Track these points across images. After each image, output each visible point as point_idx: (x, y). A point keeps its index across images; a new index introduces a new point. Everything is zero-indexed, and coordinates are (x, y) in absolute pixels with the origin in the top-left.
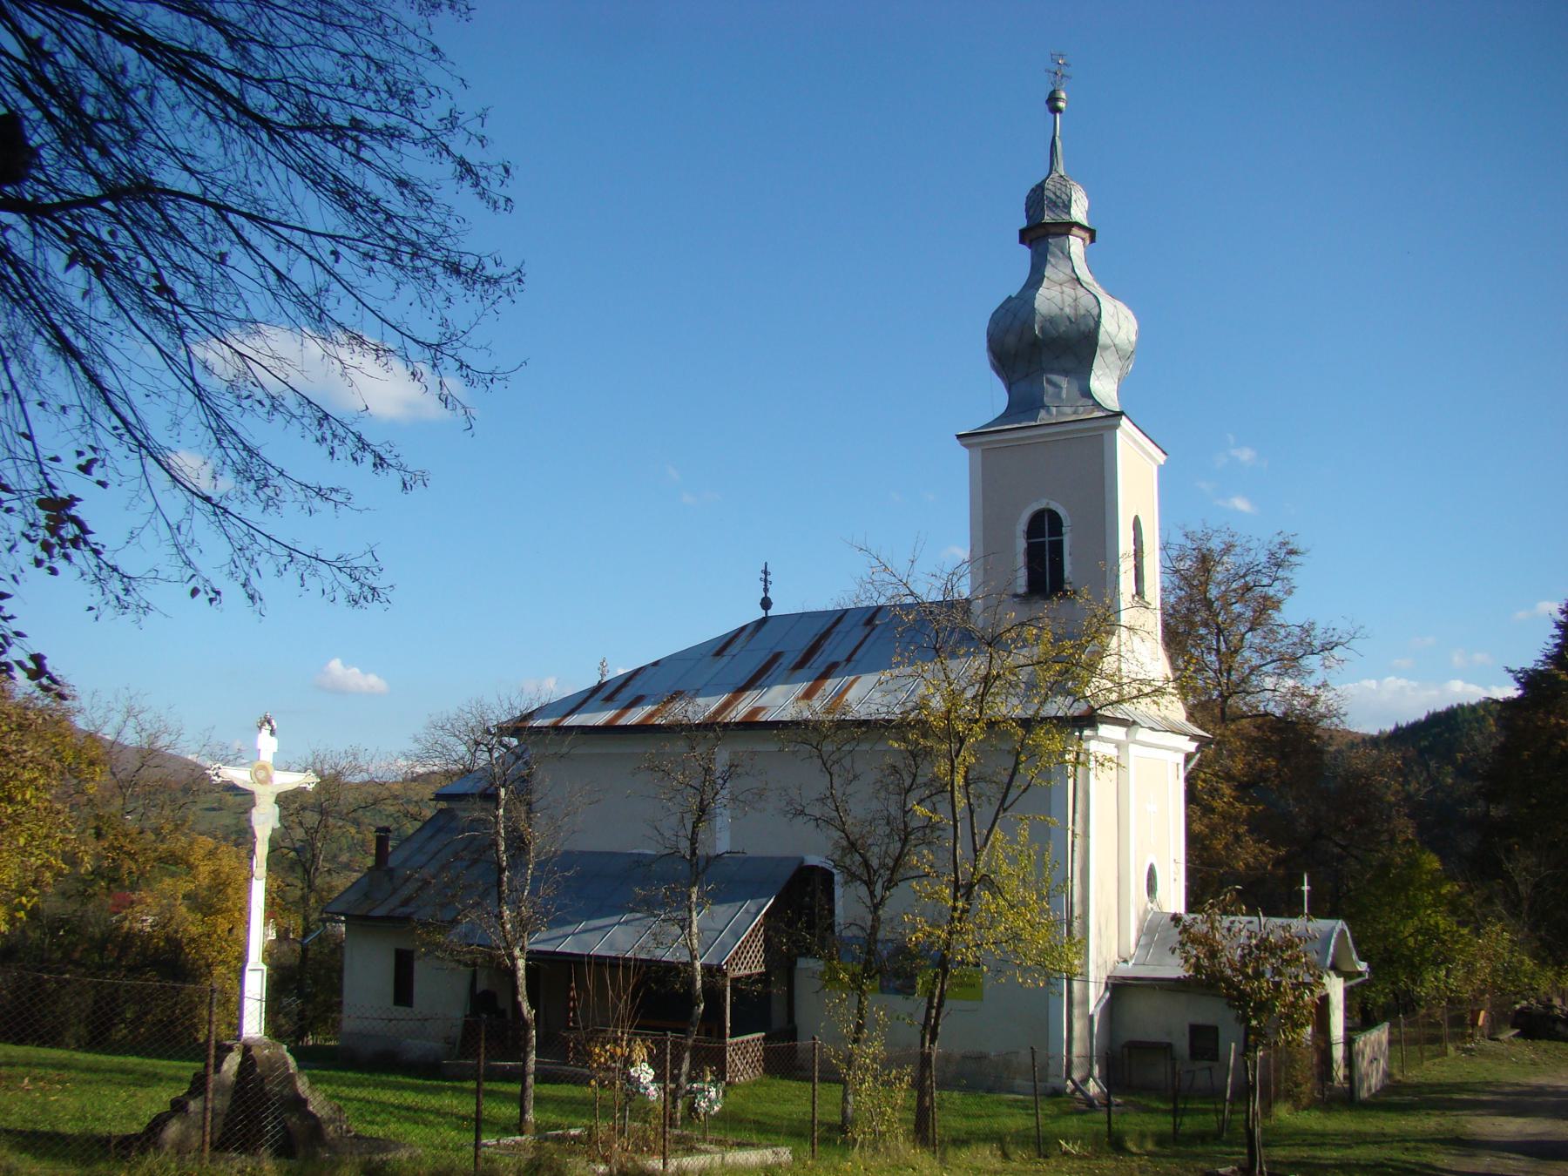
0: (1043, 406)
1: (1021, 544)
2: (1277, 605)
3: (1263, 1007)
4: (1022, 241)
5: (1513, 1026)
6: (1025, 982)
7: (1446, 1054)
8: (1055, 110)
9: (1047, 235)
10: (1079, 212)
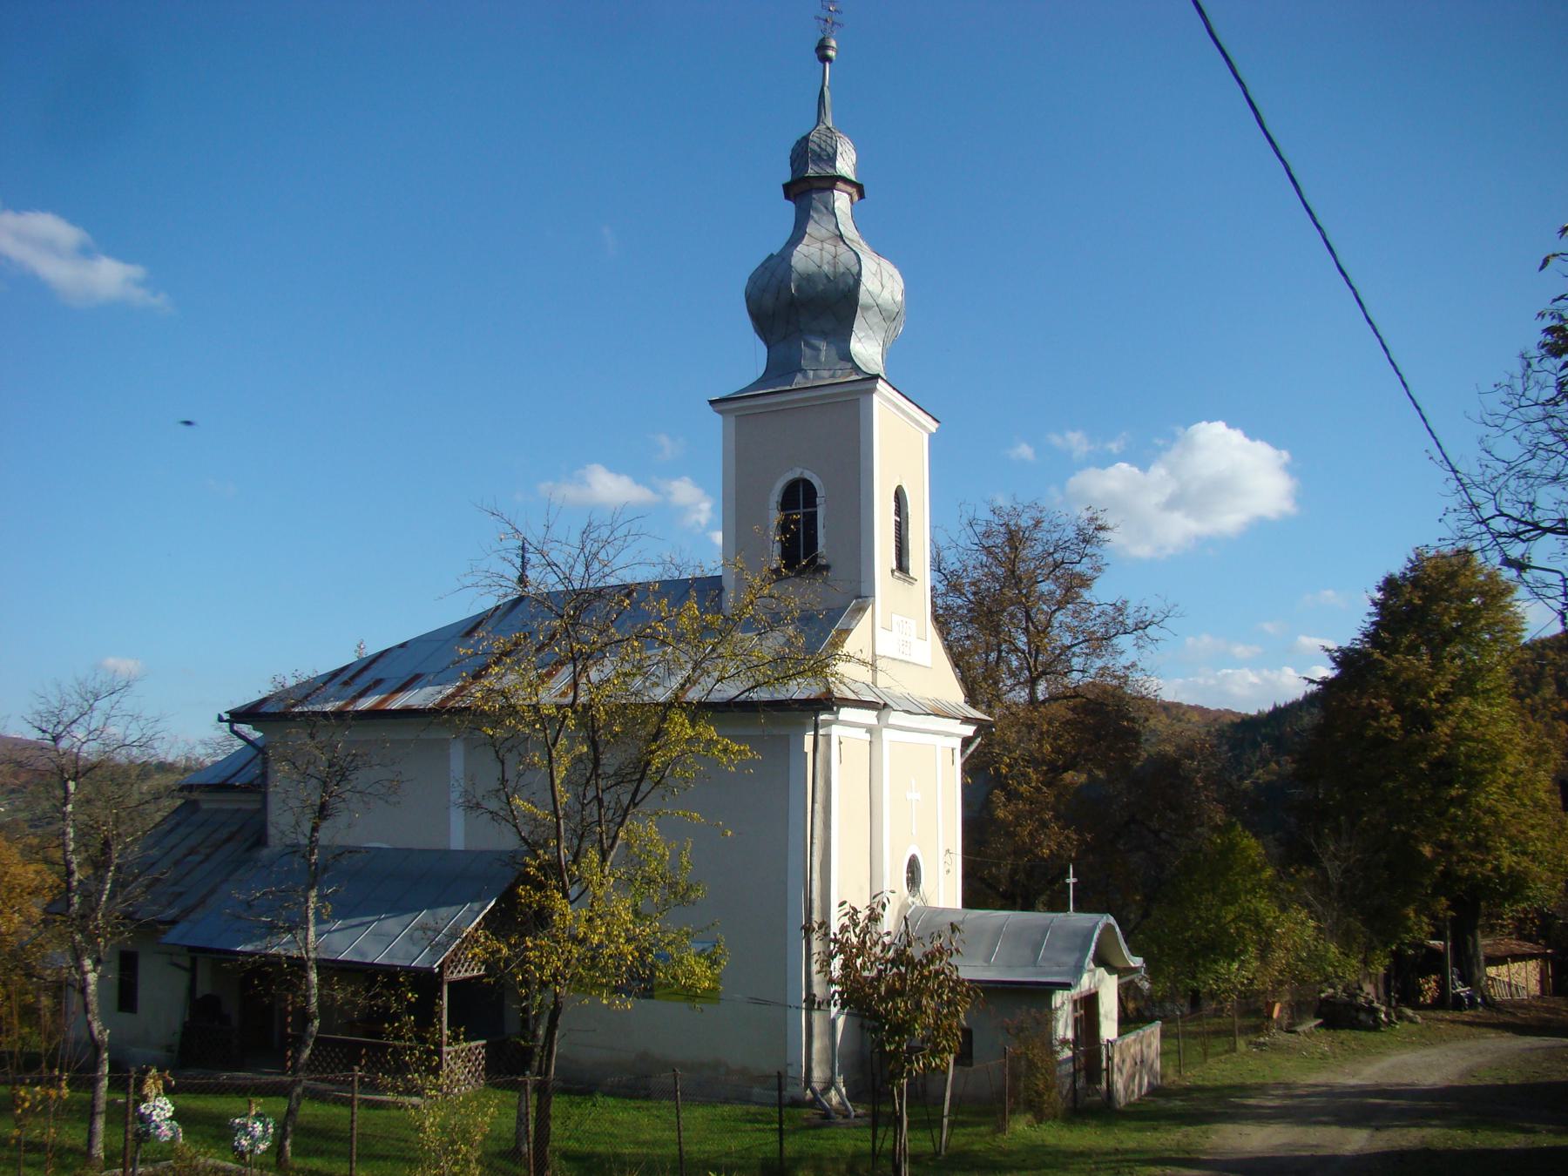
0: (801, 370)
1: (775, 517)
2: (1085, 582)
3: (902, 1028)
4: (787, 197)
5: (1317, 1016)
6: (612, 1003)
7: (1234, 1050)
8: (825, 59)
9: (810, 191)
10: (845, 164)
